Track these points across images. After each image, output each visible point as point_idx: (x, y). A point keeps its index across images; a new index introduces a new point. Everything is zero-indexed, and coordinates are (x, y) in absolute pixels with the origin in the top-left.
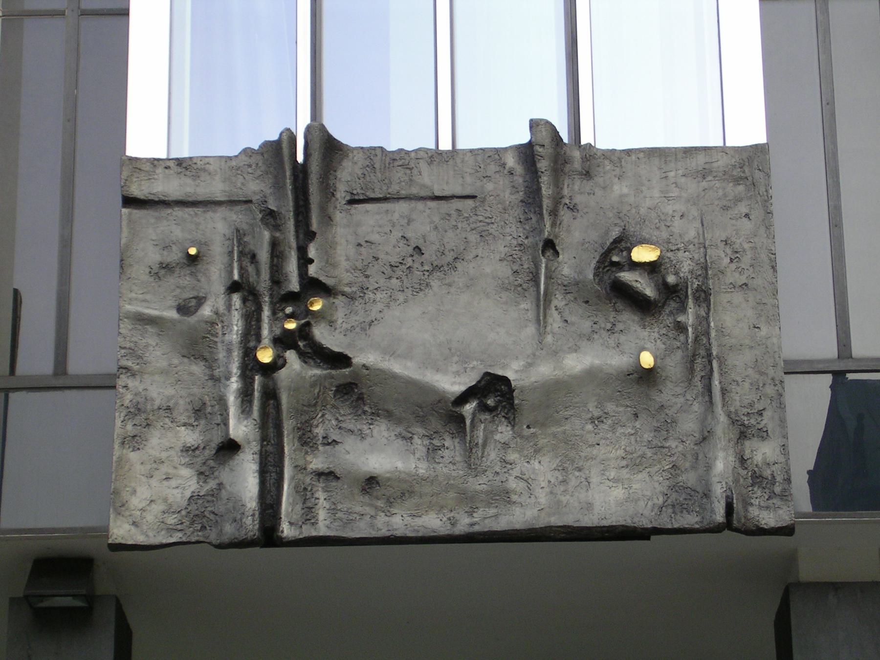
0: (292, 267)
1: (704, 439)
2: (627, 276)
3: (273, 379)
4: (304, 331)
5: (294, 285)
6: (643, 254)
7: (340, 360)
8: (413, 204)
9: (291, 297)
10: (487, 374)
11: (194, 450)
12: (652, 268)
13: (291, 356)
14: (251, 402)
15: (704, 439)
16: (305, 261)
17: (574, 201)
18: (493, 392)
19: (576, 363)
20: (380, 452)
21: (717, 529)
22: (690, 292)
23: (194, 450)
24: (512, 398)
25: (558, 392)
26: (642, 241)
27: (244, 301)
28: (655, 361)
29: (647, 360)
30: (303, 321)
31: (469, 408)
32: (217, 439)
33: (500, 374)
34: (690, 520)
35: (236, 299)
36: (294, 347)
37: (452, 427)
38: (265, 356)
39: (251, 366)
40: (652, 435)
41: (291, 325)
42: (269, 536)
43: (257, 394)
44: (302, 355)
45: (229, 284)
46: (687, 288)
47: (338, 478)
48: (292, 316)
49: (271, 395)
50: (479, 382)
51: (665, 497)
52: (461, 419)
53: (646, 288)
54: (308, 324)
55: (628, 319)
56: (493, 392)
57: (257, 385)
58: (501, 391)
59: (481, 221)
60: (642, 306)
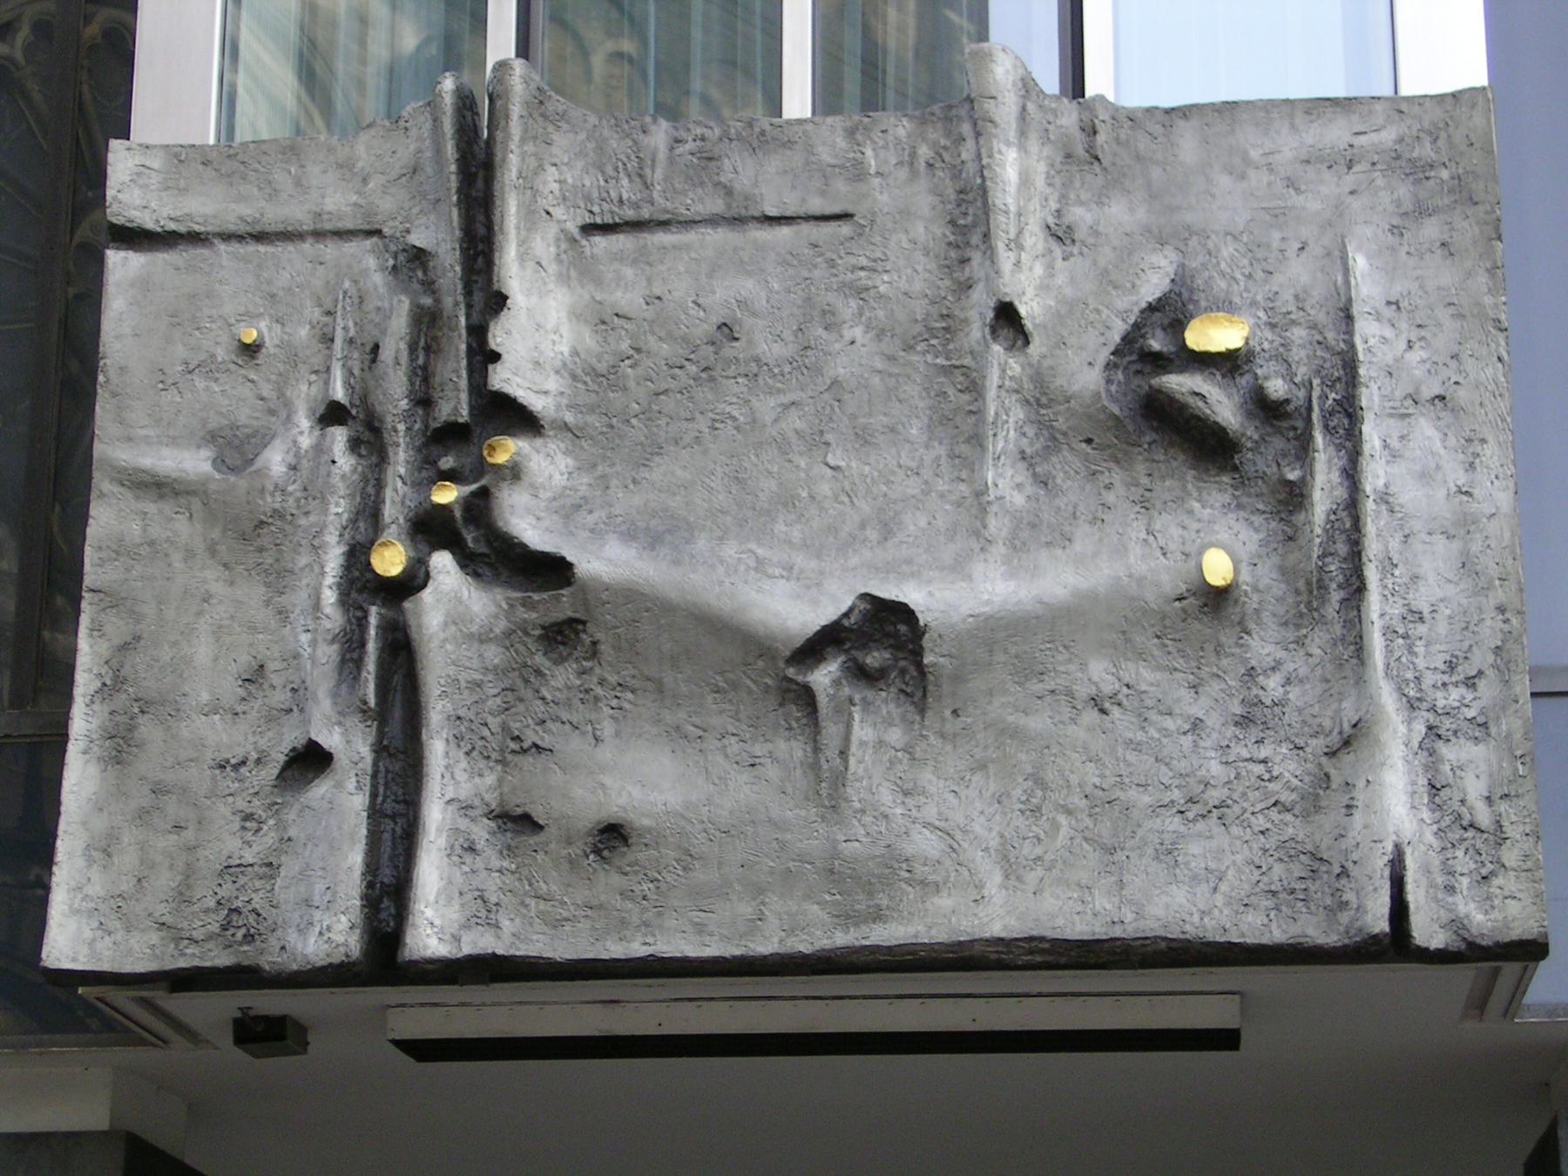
0: (454, 370)
1: (1347, 743)
2: (1179, 383)
3: (402, 612)
4: (479, 507)
5: (455, 405)
6: (1214, 334)
7: (549, 571)
8: (802, 212)
9: (452, 435)
10: (865, 597)
11: (236, 767)
12: (1227, 364)
13: (442, 562)
14: (359, 663)
15: (1347, 743)
16: (483, 356)
17: (1067, 220)
18: (881, 639)
19: (1056, 579)
20: (635, 771)
21: (1365, 951)
22: (1316, 416)
23: (236, 767)
24: (917, 654)
25: (1016, 641)
26: (1226, 306)
27: (354, 445)
28: (1236, 571)
29: (1218, 568)
30: (474, 487)
31: (824, 677)
32: (290, 738)
33: (62, 846)
34: (1315, 931)
35: (339, 436)
36: (452, 542)
37: (795, 711)
38: (390, 561)
39: (361, 584)
40: (1229, 734)
41: (446, 495)
42: (383, 956)
43: (372, 647)
44: (468, 561)
45: (321, 410)
46: (1310, 409)
47: (541, 827)
48: (452, 476)
49: (401, 651)
50: (846, 615)
51: (1257, 873)
52: (807, 698)
53: (1222, 405)
54: (484, 494)
55: (1174, 476)
56: (881, 639)
57: (373, 620)
58: (896, 635)
59: (862, 268)
60: (1209, 448)
